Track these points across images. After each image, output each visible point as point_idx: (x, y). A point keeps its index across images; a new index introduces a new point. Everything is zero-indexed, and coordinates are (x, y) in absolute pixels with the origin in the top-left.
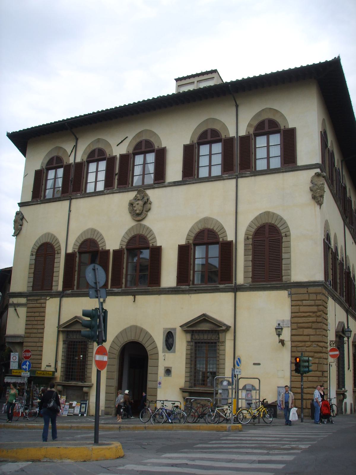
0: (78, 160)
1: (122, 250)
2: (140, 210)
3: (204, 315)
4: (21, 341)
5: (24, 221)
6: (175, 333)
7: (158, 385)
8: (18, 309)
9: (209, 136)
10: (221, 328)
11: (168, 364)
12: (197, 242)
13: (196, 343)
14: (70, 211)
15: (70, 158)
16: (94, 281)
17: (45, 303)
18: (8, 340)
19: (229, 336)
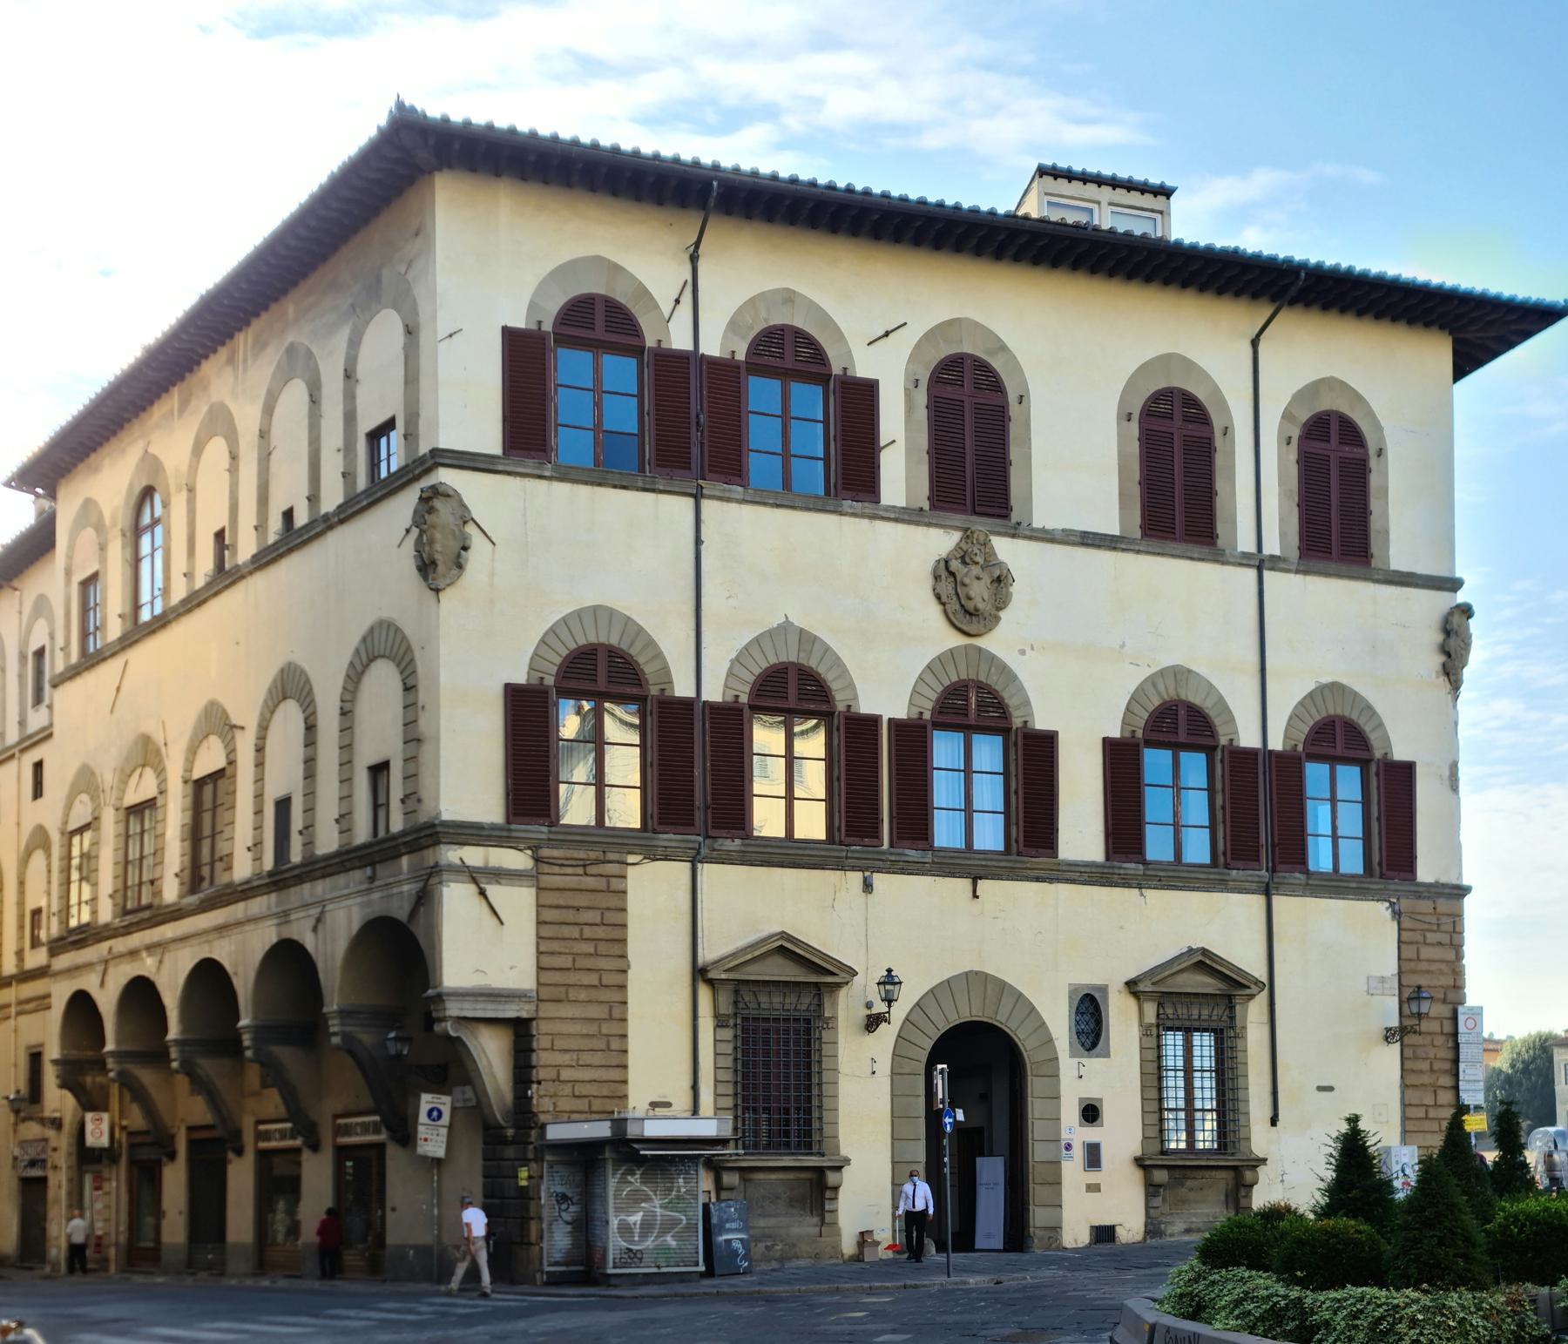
2: (969, 594)
4: (524, 1015)
5: (470, 529)
6: (1106, 998)
8: (492, 890)
9: (598, 321)
10: (1248, 992)
11: (1091, 1091)
14: (698, 542)
16: (488, 893)
18: (453, 1009)
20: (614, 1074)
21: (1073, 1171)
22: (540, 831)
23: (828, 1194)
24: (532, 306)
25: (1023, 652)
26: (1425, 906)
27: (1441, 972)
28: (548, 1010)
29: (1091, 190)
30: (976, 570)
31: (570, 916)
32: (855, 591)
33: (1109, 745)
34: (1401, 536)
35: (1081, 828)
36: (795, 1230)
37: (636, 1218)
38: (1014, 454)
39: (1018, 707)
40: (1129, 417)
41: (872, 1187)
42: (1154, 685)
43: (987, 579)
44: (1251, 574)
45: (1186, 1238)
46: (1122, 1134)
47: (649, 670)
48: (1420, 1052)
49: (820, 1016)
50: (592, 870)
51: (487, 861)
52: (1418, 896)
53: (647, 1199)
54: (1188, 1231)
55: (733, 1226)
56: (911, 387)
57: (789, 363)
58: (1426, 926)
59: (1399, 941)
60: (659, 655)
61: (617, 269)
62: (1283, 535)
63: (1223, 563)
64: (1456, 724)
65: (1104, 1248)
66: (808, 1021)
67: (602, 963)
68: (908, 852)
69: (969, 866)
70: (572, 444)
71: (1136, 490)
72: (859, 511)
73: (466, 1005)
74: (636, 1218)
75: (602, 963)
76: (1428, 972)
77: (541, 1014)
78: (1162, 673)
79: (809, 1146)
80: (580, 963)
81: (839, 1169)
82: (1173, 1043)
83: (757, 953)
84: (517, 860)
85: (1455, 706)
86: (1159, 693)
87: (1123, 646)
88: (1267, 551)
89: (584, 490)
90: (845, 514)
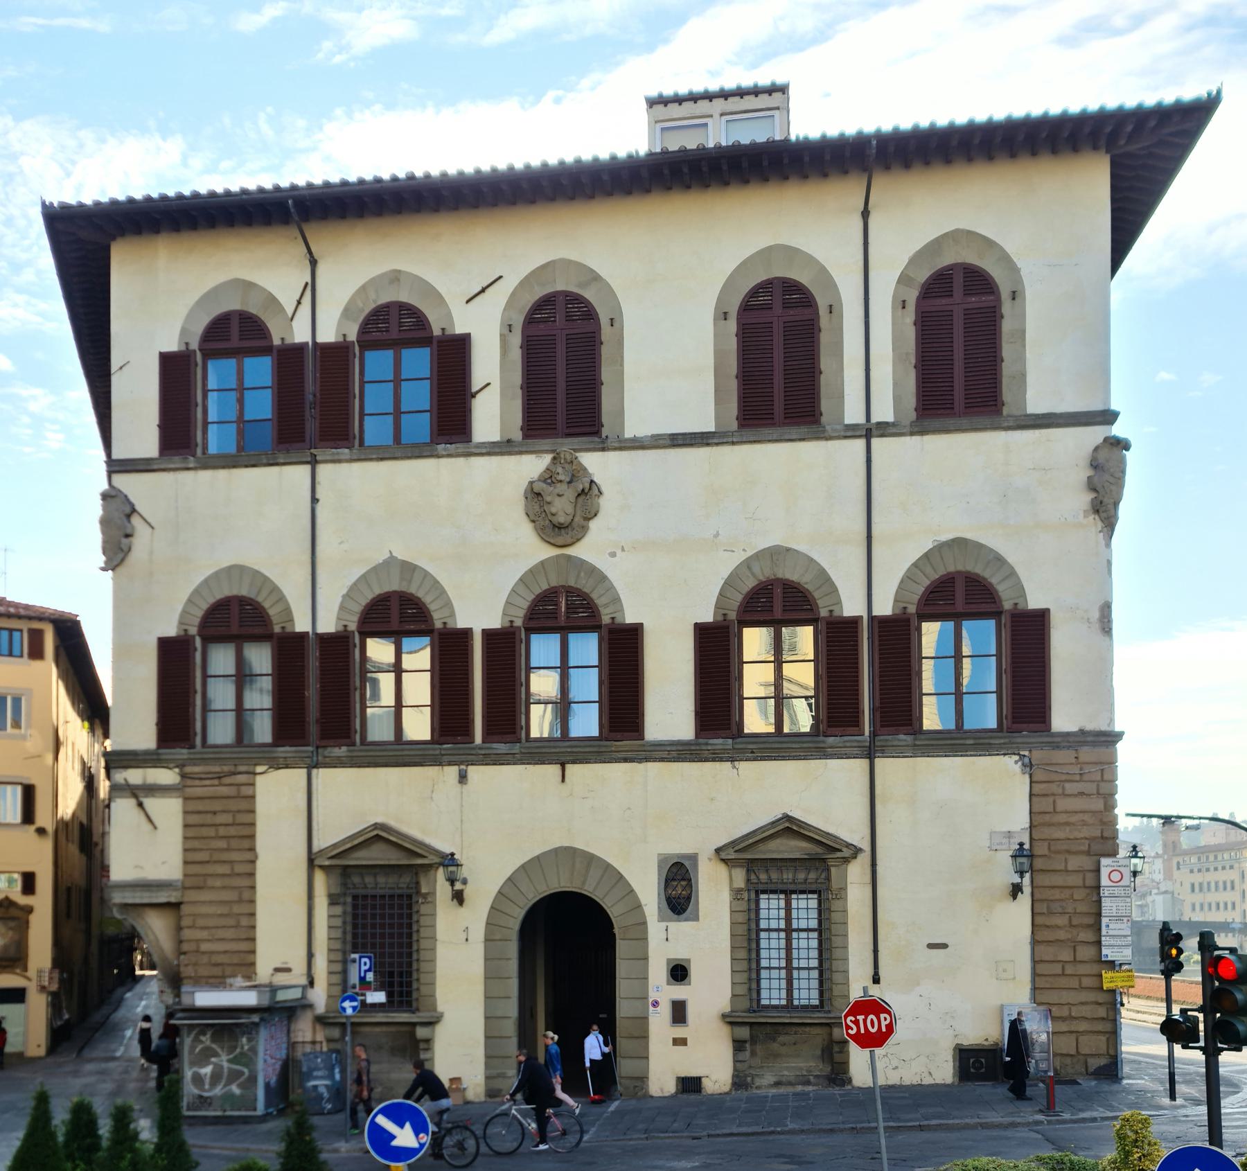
0: (327, 335)
1: (725, 623)
2: (561, 511)
3: (376, 826)
5: (135, 520)
7: (651, 1008)
8: (149, 802)
9: (235, 331)
10: (839, 854)
11: (679, 953)
12: (532, 624)
13: (355, 897)
14: (314, 500)
15: (294, 323)
17: (253, 785)
18: (118, 898)
19: (856, 872)
20: (244, 946)
21: (659, 1024)
22: (182, 753)
23: (422, 1046)
24: (184, 332)
25: (613, 555)
26: (1064, 756)
27: (1084, 823)
28: (191, 896)
29: (703, 106)
30: (561, 488)
31: (209, 819)
32: (456, 520)
33: (702, 631)
34: (1041, 371)
35: (669, 707)
36: (394, 1076)
37: (207, 1070)
38: (606, 374)
39: (606, 605)
40: (725, 316)
41: (464, 1037)
42: (749, 568)
43: (570, 494)
44: (860, 444)
45: (774, 1091)
46: (712, 991)
47: (273, 612)
48: (1056, 907)
49: (418, 892)
50: (227, 780)
51: (145, 778)
52: (1056, 747)
53: (216, 1055)
54: (777, 1084)
55: (320, 1073)
56: (506, 331)
57: (394, 334)
58: (1064, 777)
59: (1031, 795)
60: (282, 599)
61: (249, 286)
62: (897, 399)
63: (827, 439)
64: (1109, 563)
65: (743, 1094)
66: (410, 897)
67: (235, 856)
68: (495, 745)
69: (563, 752)
70: (217, 439)
71: (733, 385)
72: (452, 452)
73: (127, 894)
74: (207, 1070)
75: (235, 856)
76: (1067, 824)
77: (185, 899)
78: (758, 556)
79: (409, 1004)
80: (216, 856)
81: (431, 1024)
82: (771, 908)
83: (356, 842)
84: (166, 776)
85: (1108, 545)
86: (753, 574)
87: (717, 535)
88: (875, 419)
89: (222, 473)
90: (442, 456)
